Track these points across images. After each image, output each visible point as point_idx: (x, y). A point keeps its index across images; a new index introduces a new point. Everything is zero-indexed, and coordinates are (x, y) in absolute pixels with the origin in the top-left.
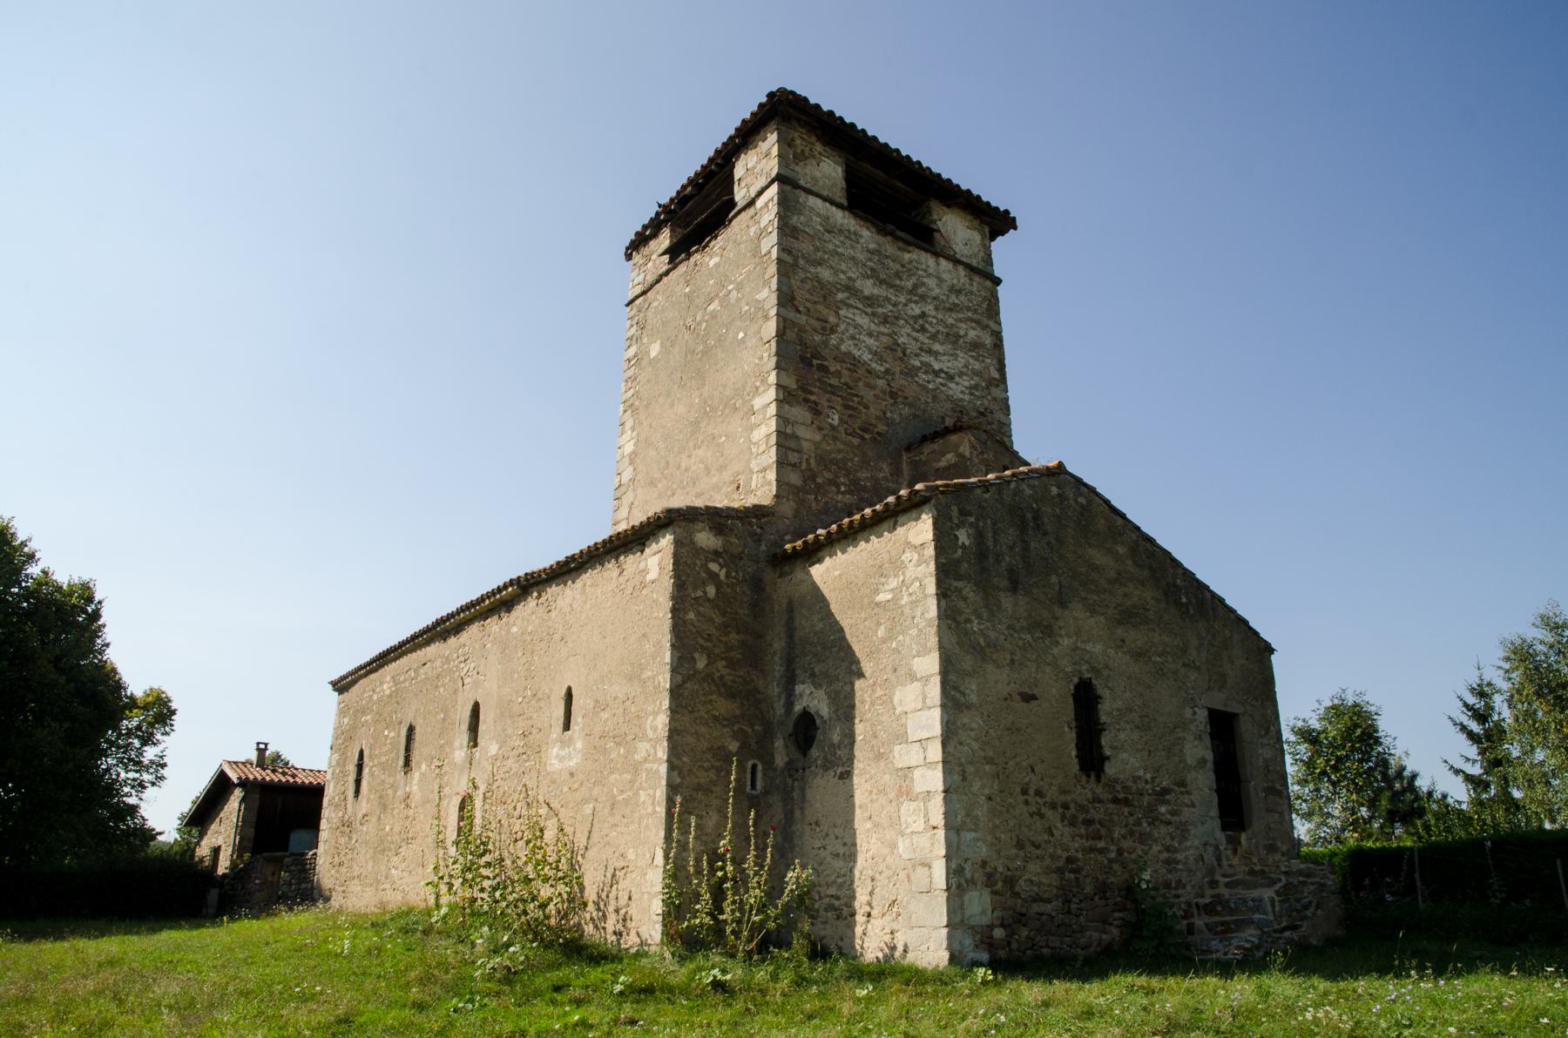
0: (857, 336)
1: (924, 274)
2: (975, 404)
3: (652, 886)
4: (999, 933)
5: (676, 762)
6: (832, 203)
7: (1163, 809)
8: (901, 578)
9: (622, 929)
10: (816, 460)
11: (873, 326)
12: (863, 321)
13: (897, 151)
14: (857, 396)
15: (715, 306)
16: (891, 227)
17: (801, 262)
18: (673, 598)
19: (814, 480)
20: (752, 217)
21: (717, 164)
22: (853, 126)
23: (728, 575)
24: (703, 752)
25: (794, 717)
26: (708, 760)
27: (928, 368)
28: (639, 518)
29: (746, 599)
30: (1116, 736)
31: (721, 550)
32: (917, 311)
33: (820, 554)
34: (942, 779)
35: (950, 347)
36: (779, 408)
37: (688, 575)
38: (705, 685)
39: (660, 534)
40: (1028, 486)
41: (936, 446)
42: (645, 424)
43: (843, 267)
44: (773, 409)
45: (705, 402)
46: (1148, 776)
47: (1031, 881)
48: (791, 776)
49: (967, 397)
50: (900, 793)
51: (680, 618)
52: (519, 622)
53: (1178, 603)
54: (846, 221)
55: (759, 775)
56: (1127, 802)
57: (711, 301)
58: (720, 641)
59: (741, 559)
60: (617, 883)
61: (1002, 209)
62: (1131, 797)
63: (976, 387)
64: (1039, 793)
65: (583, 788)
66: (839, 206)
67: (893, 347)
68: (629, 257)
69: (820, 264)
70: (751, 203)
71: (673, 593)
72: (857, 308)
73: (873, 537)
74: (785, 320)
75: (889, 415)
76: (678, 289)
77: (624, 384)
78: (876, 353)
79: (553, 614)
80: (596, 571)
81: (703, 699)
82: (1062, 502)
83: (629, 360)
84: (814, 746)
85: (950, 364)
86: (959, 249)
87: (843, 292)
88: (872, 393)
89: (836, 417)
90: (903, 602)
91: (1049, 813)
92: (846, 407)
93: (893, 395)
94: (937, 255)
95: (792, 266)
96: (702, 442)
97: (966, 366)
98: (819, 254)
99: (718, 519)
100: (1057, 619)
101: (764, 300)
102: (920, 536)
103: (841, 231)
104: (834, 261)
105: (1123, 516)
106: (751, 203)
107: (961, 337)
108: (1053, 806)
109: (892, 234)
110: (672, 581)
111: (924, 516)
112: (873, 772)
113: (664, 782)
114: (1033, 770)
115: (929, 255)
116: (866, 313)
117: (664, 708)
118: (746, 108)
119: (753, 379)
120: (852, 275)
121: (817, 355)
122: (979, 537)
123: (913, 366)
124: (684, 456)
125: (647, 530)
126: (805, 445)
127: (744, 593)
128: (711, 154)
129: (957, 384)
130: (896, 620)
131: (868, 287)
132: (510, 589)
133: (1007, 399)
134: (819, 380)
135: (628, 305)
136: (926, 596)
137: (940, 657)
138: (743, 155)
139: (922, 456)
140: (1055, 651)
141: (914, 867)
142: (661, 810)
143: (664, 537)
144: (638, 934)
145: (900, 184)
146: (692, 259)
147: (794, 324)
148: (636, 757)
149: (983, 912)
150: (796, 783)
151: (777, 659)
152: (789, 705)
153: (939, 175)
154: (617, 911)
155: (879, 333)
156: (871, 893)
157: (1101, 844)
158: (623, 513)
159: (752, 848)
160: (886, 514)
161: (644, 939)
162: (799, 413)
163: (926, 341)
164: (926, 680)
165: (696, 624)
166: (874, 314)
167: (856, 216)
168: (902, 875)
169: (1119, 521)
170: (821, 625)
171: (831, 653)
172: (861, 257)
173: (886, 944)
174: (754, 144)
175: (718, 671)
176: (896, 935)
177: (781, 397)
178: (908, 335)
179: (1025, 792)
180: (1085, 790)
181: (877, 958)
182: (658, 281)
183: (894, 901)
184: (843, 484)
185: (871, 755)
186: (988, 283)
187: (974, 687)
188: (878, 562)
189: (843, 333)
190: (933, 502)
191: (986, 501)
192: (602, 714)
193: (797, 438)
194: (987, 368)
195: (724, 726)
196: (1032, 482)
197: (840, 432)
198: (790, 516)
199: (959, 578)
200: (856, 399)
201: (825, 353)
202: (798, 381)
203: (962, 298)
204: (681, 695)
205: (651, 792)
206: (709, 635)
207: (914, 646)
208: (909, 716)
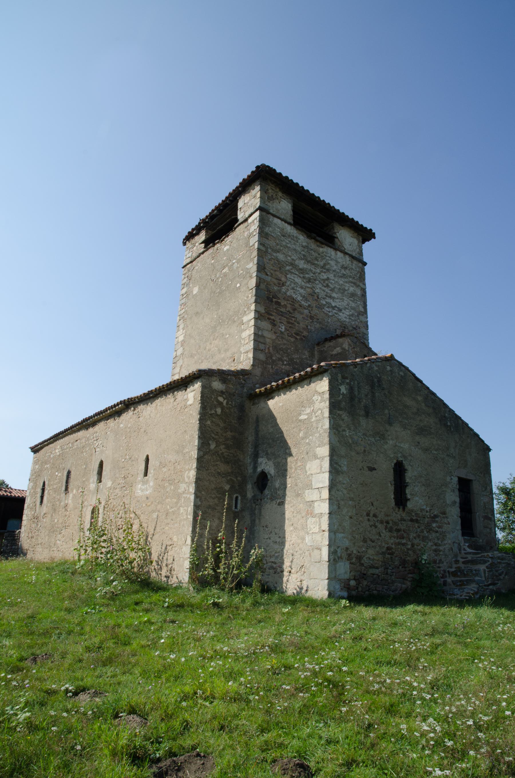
0: (295, 288)
1: (329, 259)
2: (351, 324)
4: (353, 583)
5: (199, 494)
6: (286, 222)
7: (434, 525)
8: (312, 408)
9: (169, 575)
11: (303, 283)
12: (299, 280)
14: (294, 317)
16: (314, 235)
17: (269, 250)
18: (200, 414)
19: (271, 358)
20: (246, 227)
21: (230, 200)
22: (297, 184)
23: (227, 403)
25: (257, 474)
27: (329, 305)
28: (185, 373)
29: (236, 415)
30: (413, 489)
31: (224, 391)
32: (325, 277)
34: (328, 507)
43: (290, 253)
44: (252, 322)
46: (428, 509)
47: (369, 558)
48: (255, 503)
50: (307, 513)
53: (446, 425)
54: (292, 231)
55: (239, 502)
56: (417, 521)
57: (224, 268)
58: (222, 435)
59: (234, 395)
62: (419, 519)
63: (352, 315)
64: (375, 516)
65: (153, 505)
66: (289, 223)
67: (312, 294)
68: (184, 244)
69: (278, 252)
70: (246, 220)
72: (296, 274)
73: (299, 388)
74: (260, 279)
75: (309, 327)
77: (179, 306)
78: (304, 297)
79: (141, 419)
81: (213, 463)
83: (183, 295)
85: (340, 304)
87: (289, 266)
88: (302, 316)
89: (283, 327)
90: (313, 420)
91: (379, 525)
92: (289, 323)
93: (312, 317)
94: (336, 249)
97: (348, 305)
100: (387, 431)
101: (250, 268)
103: (289, 236)
105: (421, 382)
106: (246, 220)
107: (346, 290)
108: (382, 522)
109: (314, 239)
111: (325, 379)
112: (295, 502)
113: (192, 504)
114: (372, 505)
116: (300, 277)
118: (245, 173)
119: (243, 307)
120: (294, 258)
121: (275, 297)
122: (351, 389)
123: (322, 304)
125: (188, 379)
126: (268, 340)
127: (235, 412)
128: (227, 195)
129: (343, 313)
131: (302, 264)
132: (120, 406)
133: (367, 322)
134: (276, 309)
135: (183, 268)
136: (324, 418)
137: (330, 448)
138: (243, 196)
140: (386, 447)
142: (191, 517)
143: (197, 383)
144: (177, 577)
146: (216, 247)
149: (346, 573)
151: (250, 445)
152: (255, 468)
155: (306, 287)
156: (292, 562)
157: (404, 541)
158: (177, 370)
162: (265, 325)
163: (329, 292)
164: (322, 458)
165: (211, 427)
166: (304, 277)
168: (307, 553)
169: (420, 384)
170: (272, 430)
172: (299, 249)
173: (298, 586)
176: (303, 582)
177: (257, 317)
178: (320, 288)
179: (368, 515)
180: (397, 515)
181: (293, 593)
182: (198, 257)
186: (360, 265)
187: (345, 463)
189: (288, 286)
190: (329, 371)
191: (355, 372)
192: (163, 469)
193: (264, 337)
194: (358, 306)
195: (223, 477)
196: (377, 364)
199: (340, 409)
200: (293, 319)
201: (280, 295)
202: (265, 309)
203: (347, 271)
204: (203, 461)
205: (186, 508)
206: (217, 432)
208: (313, 476)
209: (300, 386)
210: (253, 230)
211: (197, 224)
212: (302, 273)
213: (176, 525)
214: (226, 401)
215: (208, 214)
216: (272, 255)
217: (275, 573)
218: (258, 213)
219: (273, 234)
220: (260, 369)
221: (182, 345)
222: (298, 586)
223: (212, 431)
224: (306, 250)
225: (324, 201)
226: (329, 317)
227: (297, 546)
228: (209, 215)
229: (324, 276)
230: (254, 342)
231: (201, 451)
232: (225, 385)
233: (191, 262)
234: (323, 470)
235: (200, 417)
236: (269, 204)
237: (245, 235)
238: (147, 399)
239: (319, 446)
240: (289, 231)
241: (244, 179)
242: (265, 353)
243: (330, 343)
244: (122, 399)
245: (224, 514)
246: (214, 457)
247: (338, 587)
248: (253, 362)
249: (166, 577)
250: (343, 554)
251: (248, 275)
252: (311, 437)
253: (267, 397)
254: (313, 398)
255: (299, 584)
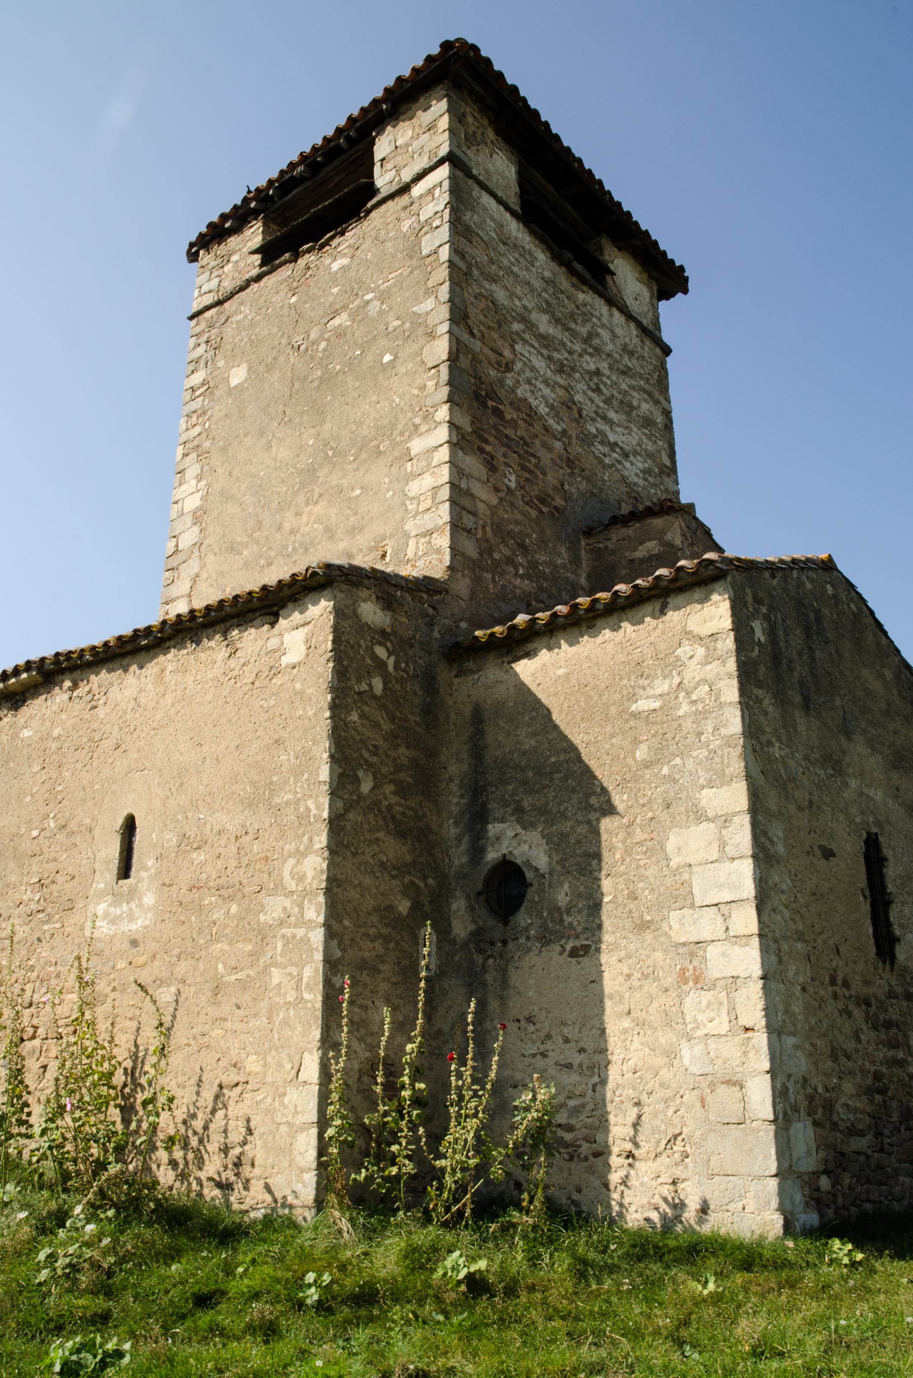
2: (649, 492)
3: (296, 1113)
4: (825, 1183)
5: (336, 927)
6: (507, 208)
8: (677, 680)
9: (233, 1178)
10: (493, 530)
11: (549, 373)
12: (539, 363)
13: (580, 161)
15: (342, 320)
16: (568, 255)
17: (476, 272)
18: (333, 689)
19: (491, 555)
20: (405, 208)
21: (348, 138)
23: (397, 666)
24: (369, 914)
25: (484, 870)
26: (374, 926)
28: (273, 575)
29: (417, 702)
31: (389, 630)
32: (592, 367)
33: (530, 646)
34: (759, 960)
35: (624, 417)
36: (453, 454)
37: (351, 660)
38: (371, 816)
39: (307, 600)
40: (808, 578)
41: (630, 532)
42: (220, 471)
43: (518, 291)
44: (444, 454)
45: (326, 444)
48: (480, 951)
49: (641, 482)
50: (682, 977)
51: (341, 719)
52: (35, 724)
54: (520, 235)
57: (336, 314)
58: (388, 756)
59: (412, 646)
60: (225, 1107)
61: (677, 264)
65: (157, 964)
66: (513, 214)
67: (569, 404)
68: (193, 257)
69: (495, 281)
70: (405, 189)
71: (332, 682)
72: (533, 347)
73: (625, 625)
74: (458, 341)
75: (566, 487)
76: (277, 299)
77: (183, 420)
78: (552, 408)
79: (101, 712)
80: (185, 651)
81: (368, 836)
82: (837, 605)
83: (193, 389)
84: (523, 908)
85: (624, 439)
86: (634, 307)
87: (519, 322)
88: (549, 456)
89: (513, 478)
90: (681, 713)
92: (523, 468)
93: (570, 463)
95: (465, 274)
96: (320, 495)
98: (494, 267)
99: (385, 586)
100: (844, 752)
101: (428, 313)
102: (709, 624)
104: (509, 281)
105: (885, 633)
106: (405, 189)
110: (331, 665)
111: (715, 597)
112: (632, 947)
113: (319, 956)
115: (603, 302)
116: (542, 356)
117: (317, 846)
119: (410, 415)
120: (527, 304)
121: (492, 395)
122: (772, 632)
123: (590, 433)
124: (289, 515)
125: (286, 592)
126: (481, 507)
127: (415, 692)
128: (342, 122)
129: (632, 464)
130: (669, 736)
132: (24, 676)
134: (495, 427)
135: (191, 318)
136: (721, 706)
137: (748, 789)
138: (389, 128)
139: (608, 544)
141: (712, 1086)
142: (315, 998)
143: (315, 603)
144: (268, 1188)
145: (570, 209)
146: (302, 262)
147: (468, 350)
148: (262, 918)
149: (809, 1153)
150: (491, 961)
151: (454, 787)
152: (477, 851)
153: (619, 204)
154: (225, 1150)
155: (555, 383)
156: (635, 1125)
158: (182, 587)
159: (470, 1056)
160: (652, 593)
161: (278, 1195)
162: (472, 463)
163: (601, 405)
164: (726, 820)
165: (360, 729)
166: (550, 358)
167: (532, 232)
168: (690, 1097)
169: (884, 641)
170: (533, 742)
171: (552, 780)
172: (537, 284)
173: (665, 1200)
174: (410, 113)
175: (386, 799)
176: (681, 1186)
177: (455, 440)
179: (833, 982)
181: (647, 1220)
182: (242, 289)
183: (676, 1137)
184: (522, 565)
185: (628, 924)
187: (780, 834)
188: (635, 657)
190: (729, 578)
192: (195, 855)
193: (472, 495)
194: (659, 451)
195: (394, 877)
197: (516, 497)
198: (466, 598)
200: (533, 461)
201: (501, 393)
202: (472, 422)
204: (343, 829)
205: (294, 971)
206: (375, 746)
207: (701, 773)
208: (695, 869)
209: (627, 620)
210: (431, 214)
211: (239, 202)
212: (546, 347)
213: (253, 1023)
214: (392, 659)
215: (275, 175)
216: (481, 286)
217: (571, 1158)
218: (444, 171)
219: (480, 233)
220: (468, 580)
221: (196, 521)
222: (665, 1200)
223: (362, 741)
224: (551, 291)
225: (590, 171)
226: (604, 468)
227: (649, 1075)
228: (277, 180)
229: (590, 364)
230: (451, 507)
231: (339, 797)
232: (389, 614)
233: (219, 303)
234: (730, 851)
235: (333, 699)
236: (469, 152)
237: (405, 229)
238: (123, 655)
239: (710, 784)
240: (514, 233)
241: (399, 79)
242: (477, 539)
243: (624, 530)
244: (35, 656)
245: (422, 984)
246: (371, 816)
247: (798, 1198)
248: (452, 560)
249: (219, 1185)
250: (799, 1097)
251: (421, 331)
252: (678, 761)
253: (508, 652)
254: (679, 652)
255: (666, 1191)
